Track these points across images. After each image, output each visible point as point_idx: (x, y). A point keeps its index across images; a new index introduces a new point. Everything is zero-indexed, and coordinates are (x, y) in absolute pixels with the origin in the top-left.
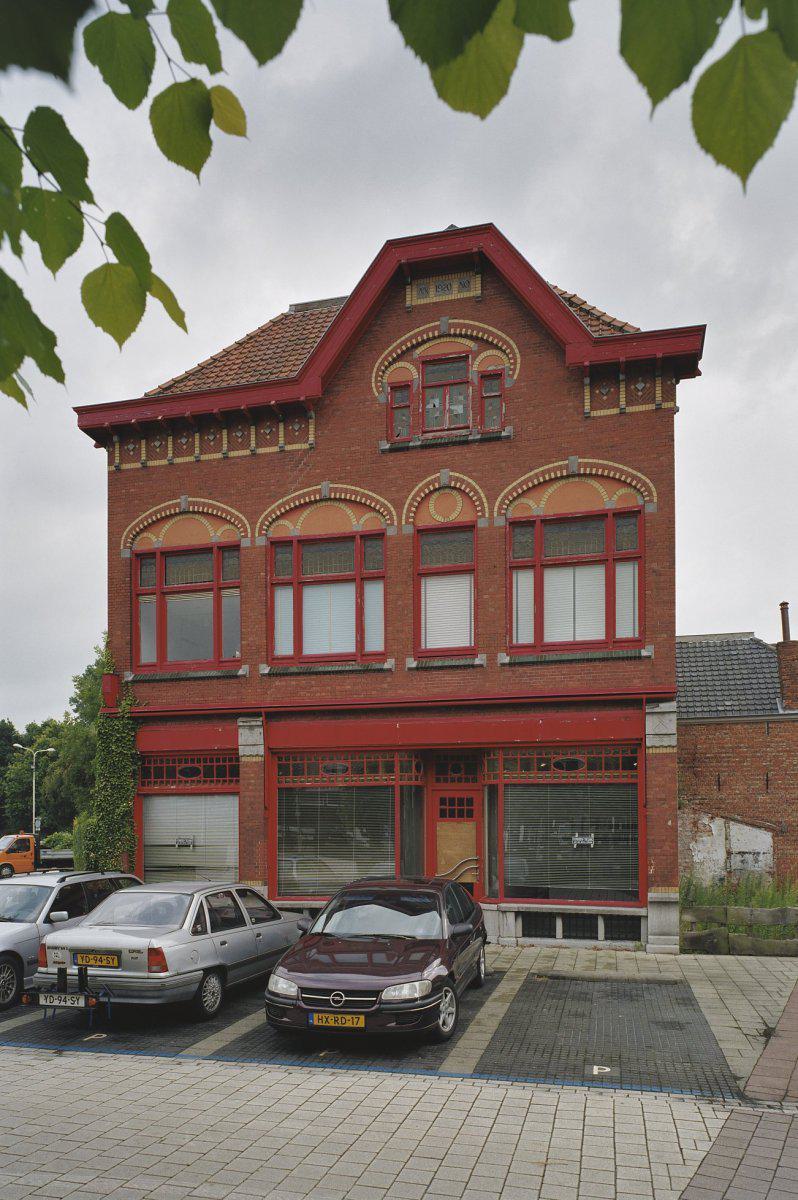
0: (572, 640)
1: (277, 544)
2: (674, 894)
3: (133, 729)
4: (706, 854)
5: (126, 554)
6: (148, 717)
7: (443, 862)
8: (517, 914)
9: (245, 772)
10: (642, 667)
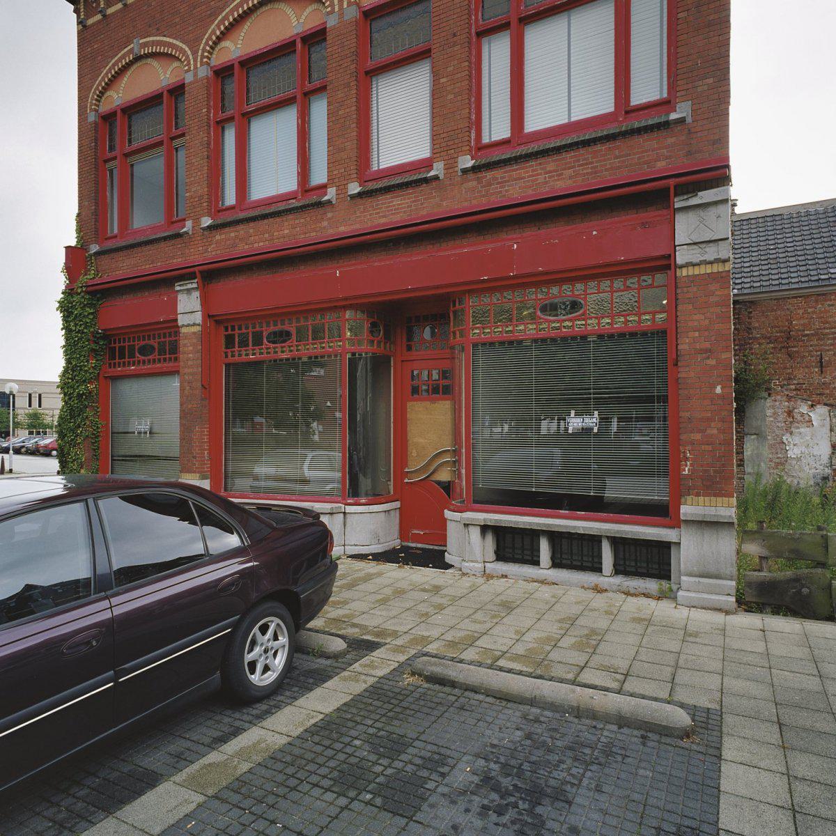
0: (566, 121)
1: (223, 73)
2: (727, 509)
3: (91, 305)
4: (803, 449)
5: (92, 117)
6: (108, 289)
7: (414, 454)
8: (485, 529)
9: (185, 345)
10: (670, 141)
